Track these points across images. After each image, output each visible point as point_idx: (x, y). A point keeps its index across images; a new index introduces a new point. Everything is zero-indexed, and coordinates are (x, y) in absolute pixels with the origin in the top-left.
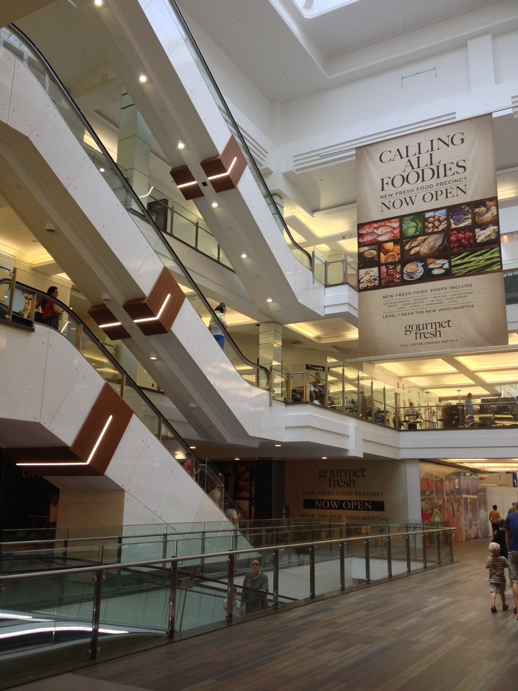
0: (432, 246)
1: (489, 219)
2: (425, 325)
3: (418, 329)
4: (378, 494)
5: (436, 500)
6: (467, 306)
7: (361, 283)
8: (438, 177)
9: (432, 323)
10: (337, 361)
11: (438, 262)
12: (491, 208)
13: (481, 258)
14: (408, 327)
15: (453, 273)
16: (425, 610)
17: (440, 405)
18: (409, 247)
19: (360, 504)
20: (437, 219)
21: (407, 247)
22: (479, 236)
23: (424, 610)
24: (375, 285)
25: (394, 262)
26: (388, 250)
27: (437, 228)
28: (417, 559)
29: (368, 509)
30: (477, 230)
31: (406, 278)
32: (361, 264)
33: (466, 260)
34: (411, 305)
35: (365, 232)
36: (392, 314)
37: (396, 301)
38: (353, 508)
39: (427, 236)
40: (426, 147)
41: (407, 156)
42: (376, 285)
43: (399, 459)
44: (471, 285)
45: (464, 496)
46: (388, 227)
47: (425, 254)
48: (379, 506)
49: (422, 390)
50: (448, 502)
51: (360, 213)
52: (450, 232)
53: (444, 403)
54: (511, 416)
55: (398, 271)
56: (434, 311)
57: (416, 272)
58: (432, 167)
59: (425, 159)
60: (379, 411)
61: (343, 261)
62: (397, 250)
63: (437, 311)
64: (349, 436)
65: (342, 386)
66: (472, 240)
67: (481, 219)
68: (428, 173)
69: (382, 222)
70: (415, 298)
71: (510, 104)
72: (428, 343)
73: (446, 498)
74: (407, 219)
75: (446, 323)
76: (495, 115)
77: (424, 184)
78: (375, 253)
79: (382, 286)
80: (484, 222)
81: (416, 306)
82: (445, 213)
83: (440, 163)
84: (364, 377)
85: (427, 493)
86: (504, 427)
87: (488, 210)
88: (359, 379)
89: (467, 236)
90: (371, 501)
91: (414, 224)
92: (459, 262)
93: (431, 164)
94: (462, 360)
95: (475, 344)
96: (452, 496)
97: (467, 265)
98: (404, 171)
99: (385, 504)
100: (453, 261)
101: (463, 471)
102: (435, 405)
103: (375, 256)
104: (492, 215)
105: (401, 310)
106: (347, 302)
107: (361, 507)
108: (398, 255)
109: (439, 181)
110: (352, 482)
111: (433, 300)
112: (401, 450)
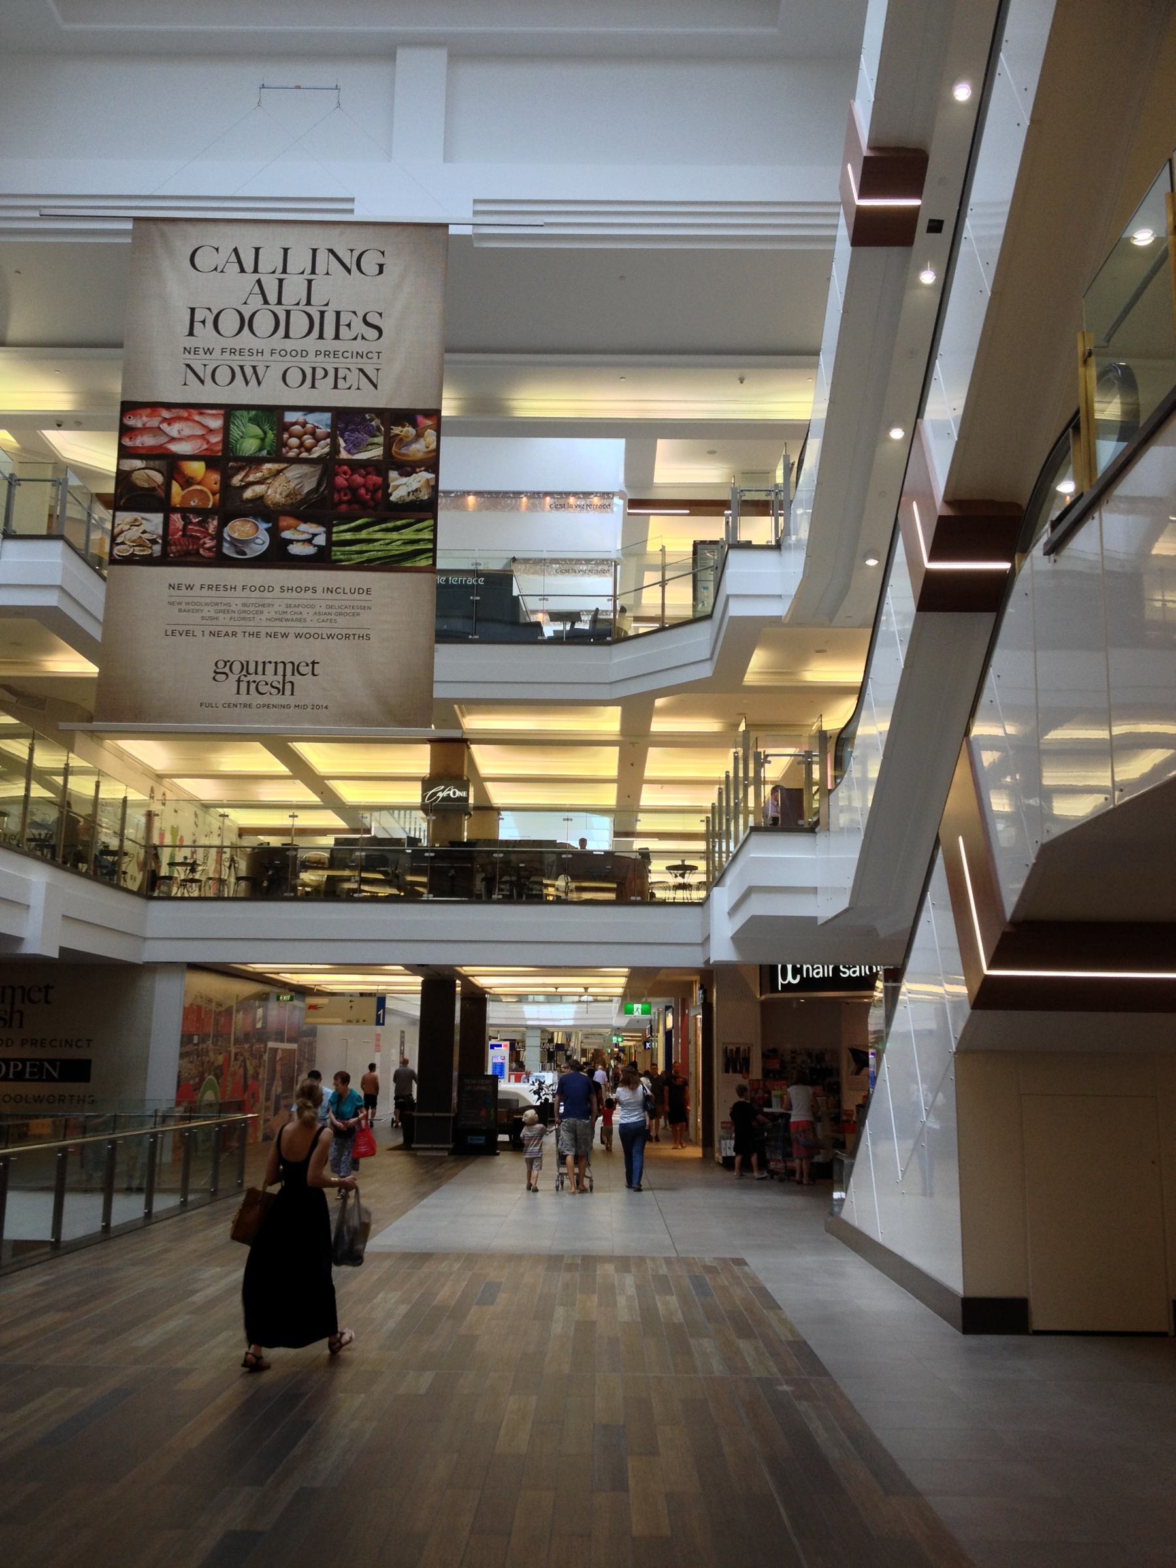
0: (294, 488)
1: (420, 455)
2: (262, 664)
3: (244, 672)
4: (80, 1044)
5: (211, 1054)
6: (356, 636)
7: (118, 544)
8: (321, 337)
9: (276, 663)
11: (303, 527)
12: (426, 433)
13: (395, 535)
14: (221, 664)
15: (334, 558)
16: (198, 1298)
17: (239, 845)
18: (241, 481)
19: (32, 1066)
20: (310, 430)
21: (236, 480)
22: (397, 487)
23: (194, 1298)
24: (151, 555)
25: (203, 509)
26: (192, 478)
27: (309, 450)
28: (162, 1187)
29: (50, 1078)
30: (393, 474)
31: (227, 550)
32: (121, 500)
33: (363, 535)
34: (233, 615)
35: (139, 425)
36: (187, 628)
37: (198, 600)
38: (11, 1076)
39: (286, 465)
40: (299, 260)
41: (256, 271)
42: (155, 555)
43: (140, 962)
44: (368, 591)
46: (195, 425)
47: (277, 504)
48: (78, 1071)
49: (204, 809)
50: (236, 1059)
51: (129, 375)
52: (337, 467)
53: (250, 841)
54: (380, 876)
55: (210, 531)
56: (285, 635)
57: (253, 541)
58: (308, 309)
59: (295, 289)
60: (106, 851)
61: (55, 483)
62: (213, 482)
63: (291, 636)
64: (28, 906)
65: (24, 785)
66: (380, 494)
67: (403, 451)
68: (299, 323)
69: (182, 410)
70: (244, 601)
71: (468, 216)
72: (264, 706)
73: (233, 1050)
74: (242, 416)
75: (307, 665)
76: (453, 230)
77: (289, 345)
78: (158, 478)
79: (170, 559)
80: (409, 459)
81: (244, 619)
82: (329, 422)
83: (327, 305)
84: (74, 769)
86: (374, 899)
87: (419, 435)
88: (66, 771)
89: (370, 483)
90: (58, 1060)
91: (259, 432)
92: (348, 536)
93: (308, 303)
94: (309, 751)
95: (364, 719)
96: (246, 1046)
97: (364, 547)
98: (245, 303)
99: (93, 1065)
100: (337, 532)
101: (276, 990)
102: (229, 844)
103: (159, 486)
104: (427, 447)
105: (209, 622)
106: (58, 583)
107: (32, 1073)
108: (214, 494)
109: (322, 345)
110: (17, 1016)
111: (285, 609)
112: (149, 943)
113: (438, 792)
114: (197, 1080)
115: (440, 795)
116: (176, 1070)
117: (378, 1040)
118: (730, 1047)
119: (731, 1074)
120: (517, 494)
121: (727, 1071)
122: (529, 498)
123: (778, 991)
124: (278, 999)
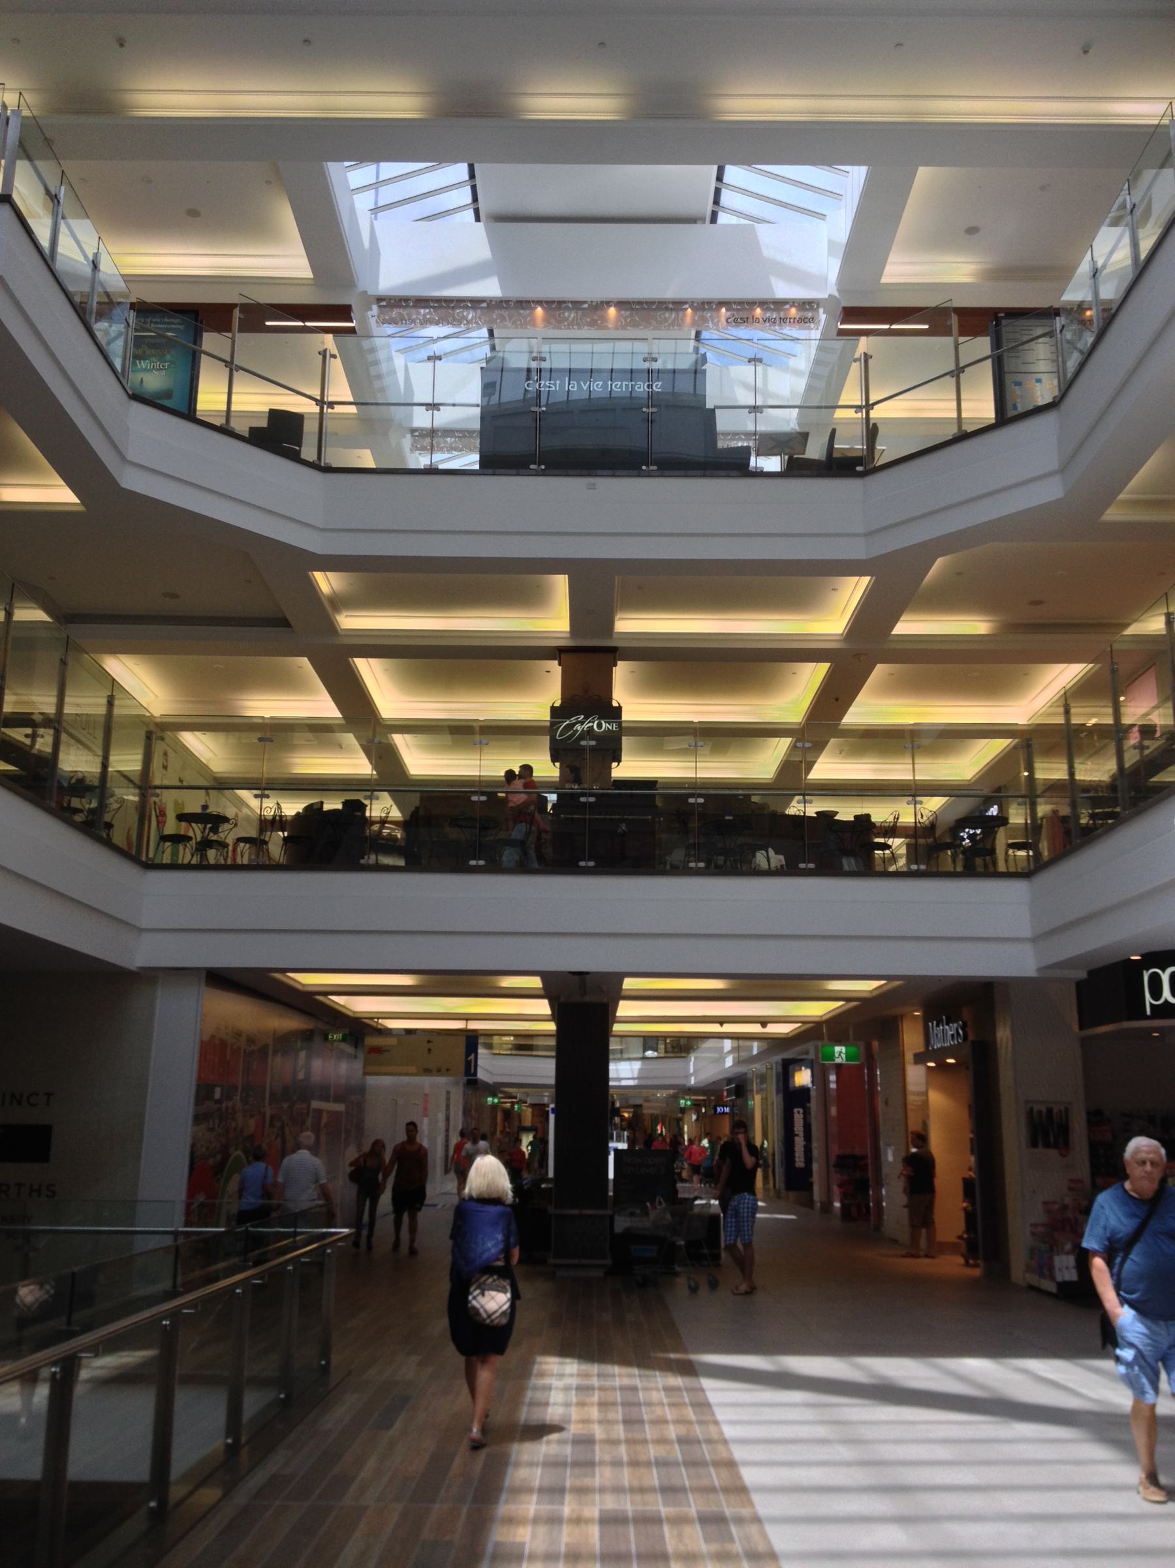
10: (50, 620)
45: (315, 1104)
50: (272, 1125)
85: (218, 1093)
96: (285, 1106)
113: (574, 724)
114: (219, 1157)
115: (579, 727)
116: (189, 1141)
117: (426, 1101)
118: (1036, 1107)
119: (1041, 1150)
120: (678, 305)
121: (1034, 1144)
122: (694, 309)
123: (1144, 1016)
124: (326, 1038)
